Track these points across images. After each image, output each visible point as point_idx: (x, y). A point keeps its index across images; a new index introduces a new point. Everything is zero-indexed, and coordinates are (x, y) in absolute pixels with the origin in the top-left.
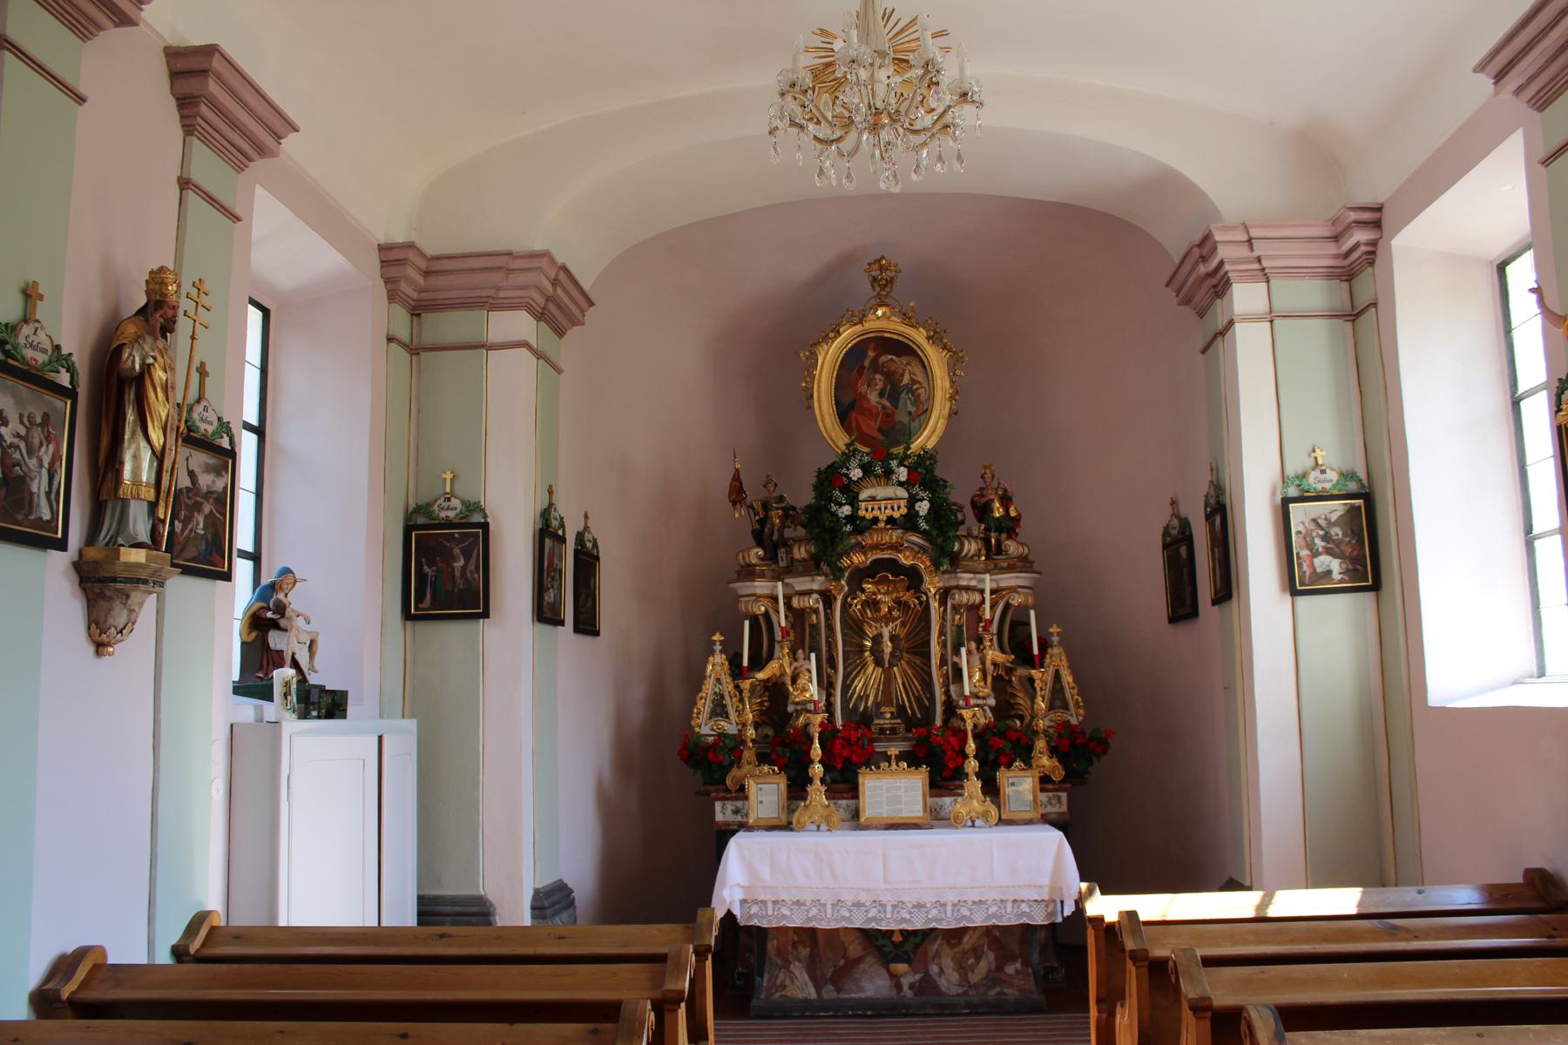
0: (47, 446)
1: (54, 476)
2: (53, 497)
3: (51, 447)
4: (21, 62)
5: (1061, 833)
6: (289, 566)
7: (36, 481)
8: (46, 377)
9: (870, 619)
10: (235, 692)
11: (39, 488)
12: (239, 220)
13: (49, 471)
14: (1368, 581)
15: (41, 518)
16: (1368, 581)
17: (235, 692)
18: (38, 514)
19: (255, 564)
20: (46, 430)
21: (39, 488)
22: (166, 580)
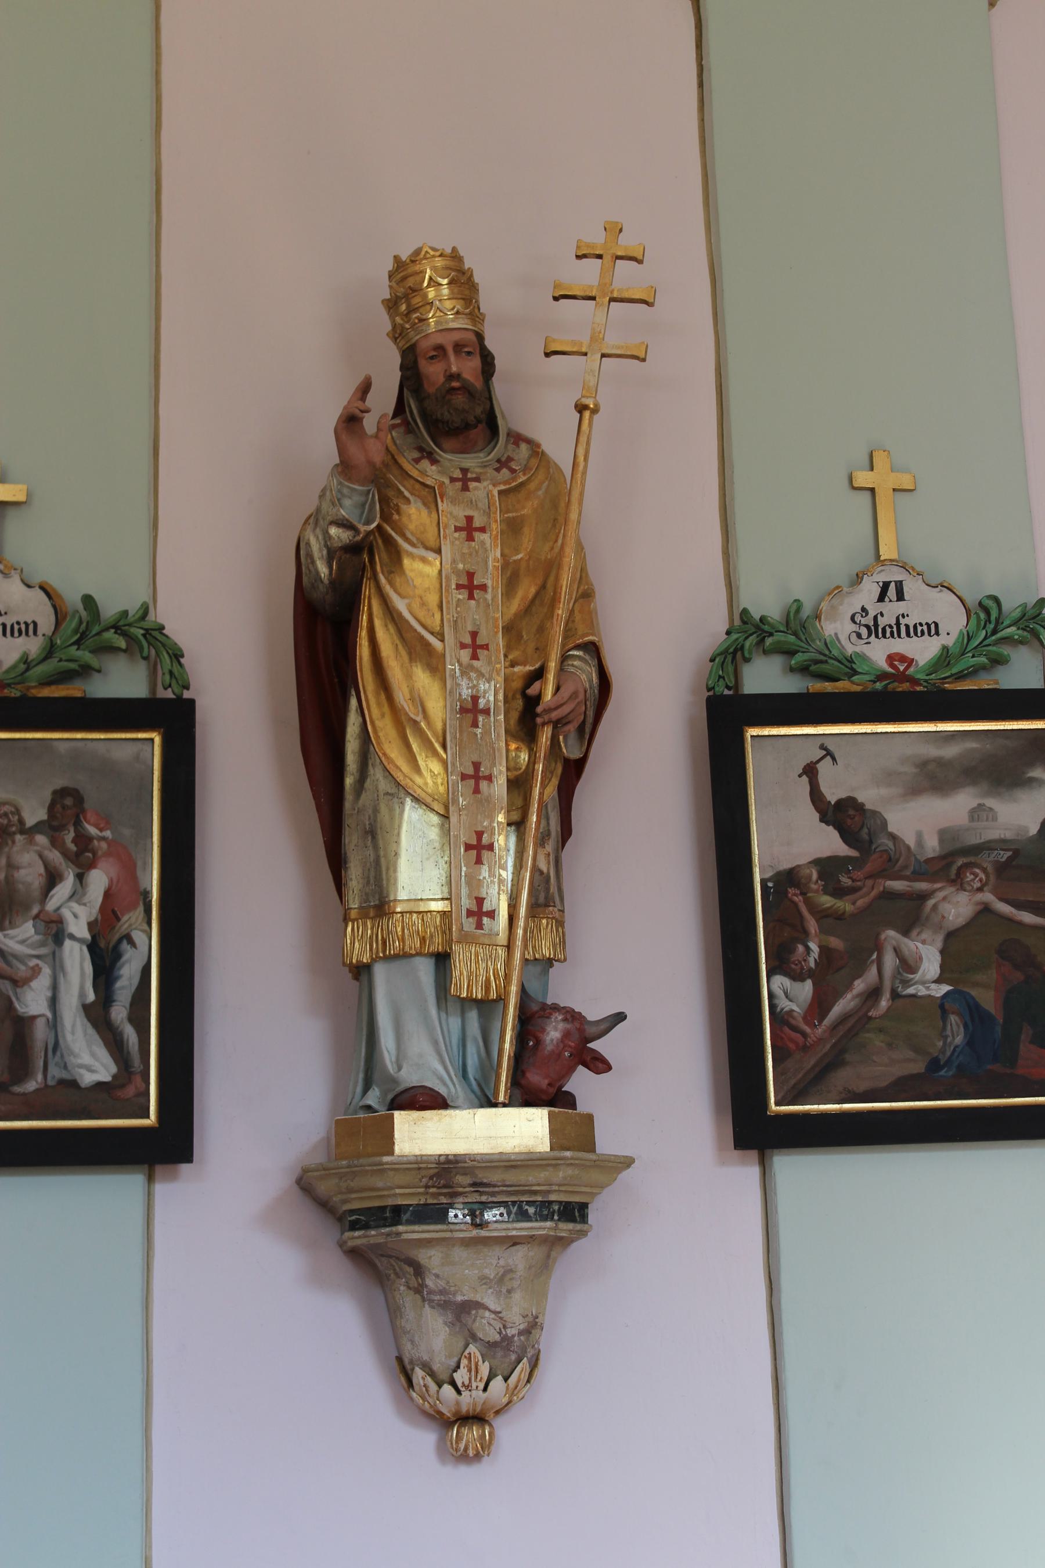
0: (80, 877)
1: (116, 955)
2: (119, 1013)
3: (98, 881)
4: (160, 513)
5: (939, 972)
6: (600, 413)
7: (41, 985)
8: (30, 695)
9: (820, 1005)
10: (395, 257)
11: (54, 1002)
12: (608, 1068)
13: (93, 948)
14: (777, 1104)
15: (72, 1084)
16: (777, 1104)
17: (395, 257)
18: (56, 1073)
19: (506, 468)
20: (69, 836)
21: (54, 1002)
22: (593, 1195)
